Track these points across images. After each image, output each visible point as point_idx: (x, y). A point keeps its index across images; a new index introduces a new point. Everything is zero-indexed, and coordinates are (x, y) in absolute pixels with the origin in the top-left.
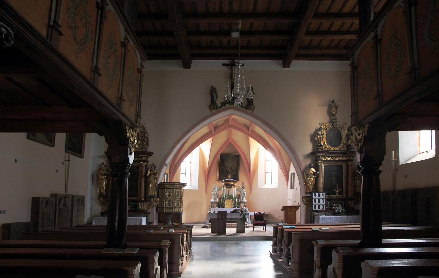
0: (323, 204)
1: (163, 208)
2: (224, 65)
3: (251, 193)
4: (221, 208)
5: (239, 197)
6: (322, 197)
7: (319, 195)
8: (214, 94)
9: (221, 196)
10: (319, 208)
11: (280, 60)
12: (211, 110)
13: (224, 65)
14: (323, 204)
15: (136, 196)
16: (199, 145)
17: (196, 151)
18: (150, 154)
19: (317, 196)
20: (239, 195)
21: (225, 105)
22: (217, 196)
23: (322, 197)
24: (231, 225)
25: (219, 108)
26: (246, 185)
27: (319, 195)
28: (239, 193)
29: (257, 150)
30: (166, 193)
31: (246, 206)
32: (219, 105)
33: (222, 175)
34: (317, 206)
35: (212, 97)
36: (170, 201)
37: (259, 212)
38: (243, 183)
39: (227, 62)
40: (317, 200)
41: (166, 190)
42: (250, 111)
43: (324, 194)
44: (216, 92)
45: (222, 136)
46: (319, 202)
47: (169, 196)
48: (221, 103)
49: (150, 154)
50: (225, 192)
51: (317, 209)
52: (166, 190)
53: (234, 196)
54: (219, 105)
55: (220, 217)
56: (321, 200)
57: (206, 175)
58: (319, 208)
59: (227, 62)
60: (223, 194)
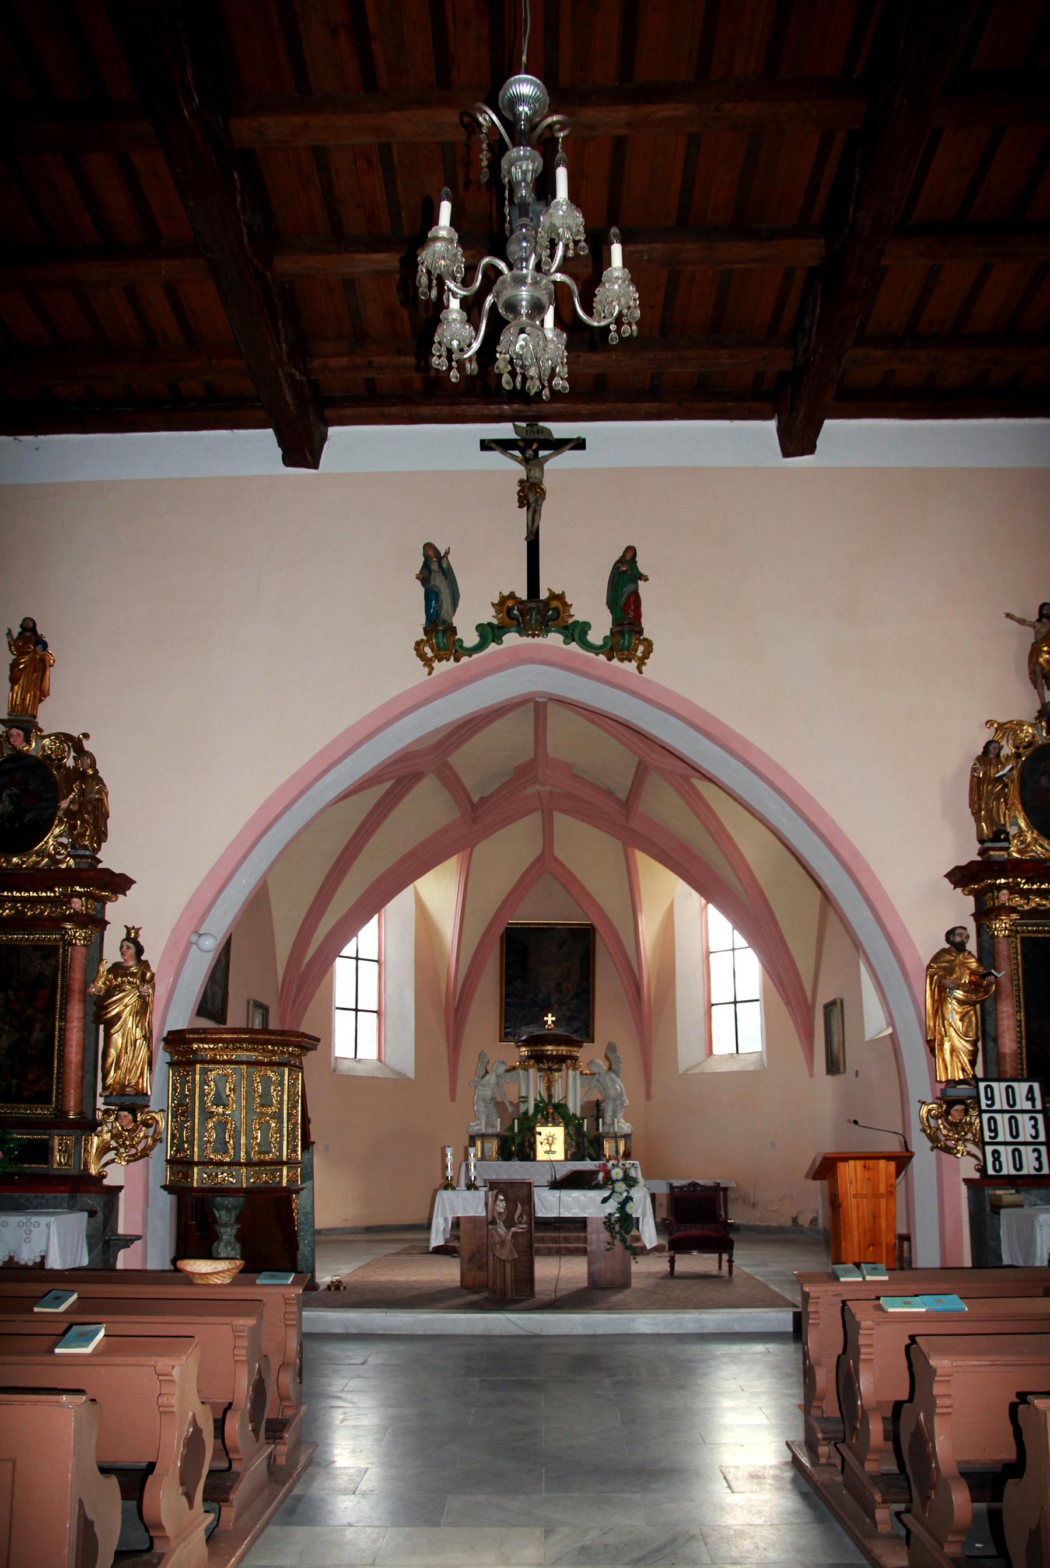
0: (1034, 1143)
1: (192, 1164)
2: (486, 445)
3: (648, 1096)
4: (516, 1164)
5: (596, 1110)
6: (1028, 1105)
7: (1010, 1091)
8: (439, 581)
9: (517, 1106)
10: (1018, 1165)
11: (770, 418)
12: (428, 663)
13: (486, 445)
14: (1034, 1143)
15: (44, 1098)
16: (412, 881)
17: (401, 905)
18: (120, 884)
19: (1000, 1103)
20: (598, 1104)
21: (498, 639)
22: (499, 1106)
23: (1028, 1105)
24: (566, 1240)
25: (471, 652)
26: (628, 1054)
27: (1010, 1091)
28: (596, 1096)
29: (664, 909)
30: (205, 1082)
31: (627, 1155)
32: (469, 637)
33: (518, 1010)
34: (1006, 1152)
35: (431, 596)
36: (221, 1126)
37: (694, 1185)
38: (611, 1048)
39: (505, 430)
40: (1002, 1120)
41: (204, 1072)
42: (631, 666)
43: (1036, 1086)
44: (448, 574)
45: (510, 850)
46: (1015, 1133)
47: (219, 1101)
48: (480, 628)
49: (120, 884)
50: (532, 1086)
51: (1008, 1169)
52: (204, 1072)
53: (574, 1107)
54: (469, 637)
55: (501, 1207)
56: (1024, 1120)
57: (443, 1012)
58: (1018, 1165)
59: (505, 430)
60: (525, 1099)
